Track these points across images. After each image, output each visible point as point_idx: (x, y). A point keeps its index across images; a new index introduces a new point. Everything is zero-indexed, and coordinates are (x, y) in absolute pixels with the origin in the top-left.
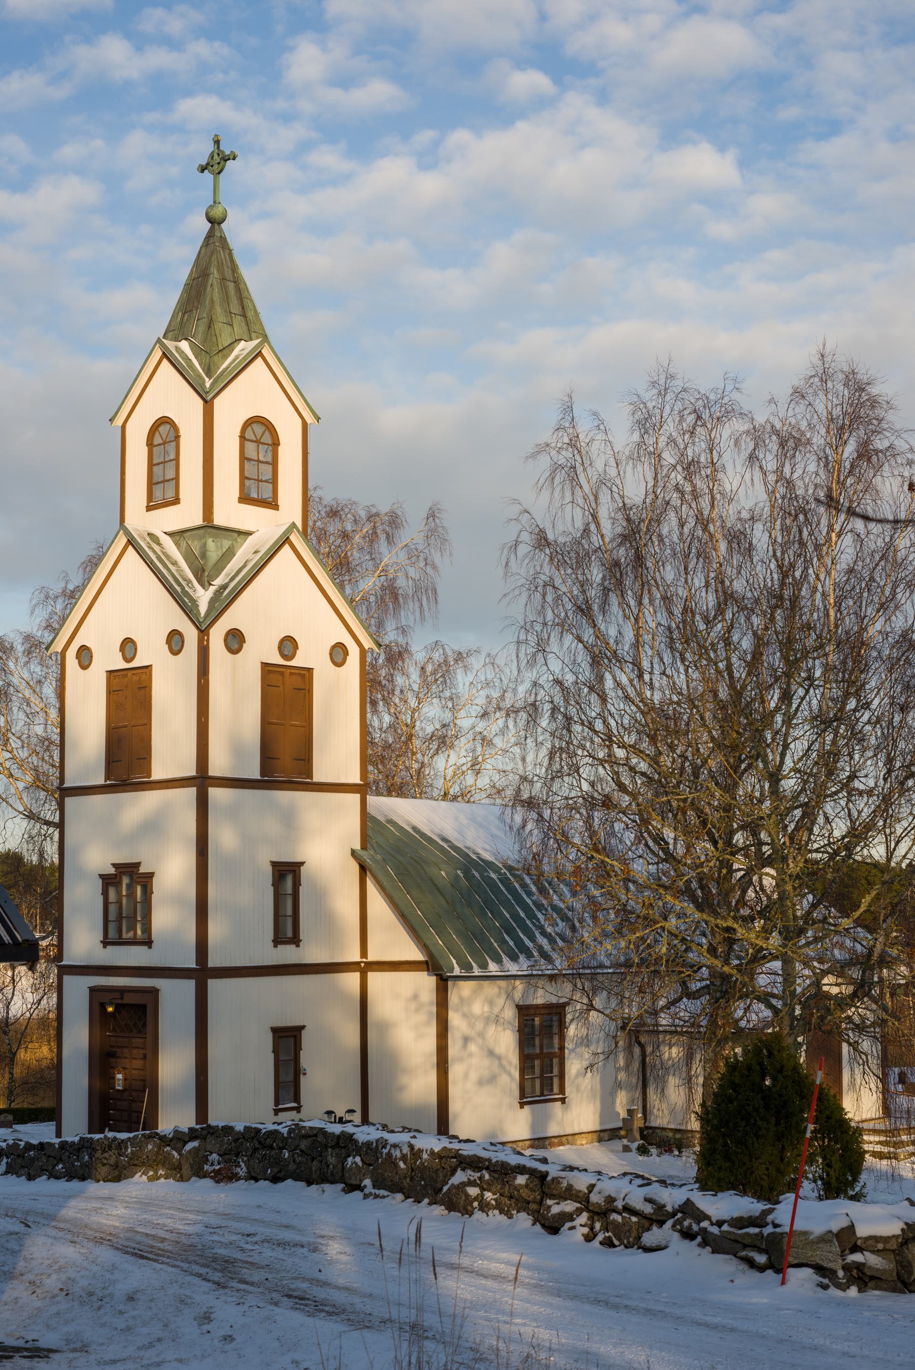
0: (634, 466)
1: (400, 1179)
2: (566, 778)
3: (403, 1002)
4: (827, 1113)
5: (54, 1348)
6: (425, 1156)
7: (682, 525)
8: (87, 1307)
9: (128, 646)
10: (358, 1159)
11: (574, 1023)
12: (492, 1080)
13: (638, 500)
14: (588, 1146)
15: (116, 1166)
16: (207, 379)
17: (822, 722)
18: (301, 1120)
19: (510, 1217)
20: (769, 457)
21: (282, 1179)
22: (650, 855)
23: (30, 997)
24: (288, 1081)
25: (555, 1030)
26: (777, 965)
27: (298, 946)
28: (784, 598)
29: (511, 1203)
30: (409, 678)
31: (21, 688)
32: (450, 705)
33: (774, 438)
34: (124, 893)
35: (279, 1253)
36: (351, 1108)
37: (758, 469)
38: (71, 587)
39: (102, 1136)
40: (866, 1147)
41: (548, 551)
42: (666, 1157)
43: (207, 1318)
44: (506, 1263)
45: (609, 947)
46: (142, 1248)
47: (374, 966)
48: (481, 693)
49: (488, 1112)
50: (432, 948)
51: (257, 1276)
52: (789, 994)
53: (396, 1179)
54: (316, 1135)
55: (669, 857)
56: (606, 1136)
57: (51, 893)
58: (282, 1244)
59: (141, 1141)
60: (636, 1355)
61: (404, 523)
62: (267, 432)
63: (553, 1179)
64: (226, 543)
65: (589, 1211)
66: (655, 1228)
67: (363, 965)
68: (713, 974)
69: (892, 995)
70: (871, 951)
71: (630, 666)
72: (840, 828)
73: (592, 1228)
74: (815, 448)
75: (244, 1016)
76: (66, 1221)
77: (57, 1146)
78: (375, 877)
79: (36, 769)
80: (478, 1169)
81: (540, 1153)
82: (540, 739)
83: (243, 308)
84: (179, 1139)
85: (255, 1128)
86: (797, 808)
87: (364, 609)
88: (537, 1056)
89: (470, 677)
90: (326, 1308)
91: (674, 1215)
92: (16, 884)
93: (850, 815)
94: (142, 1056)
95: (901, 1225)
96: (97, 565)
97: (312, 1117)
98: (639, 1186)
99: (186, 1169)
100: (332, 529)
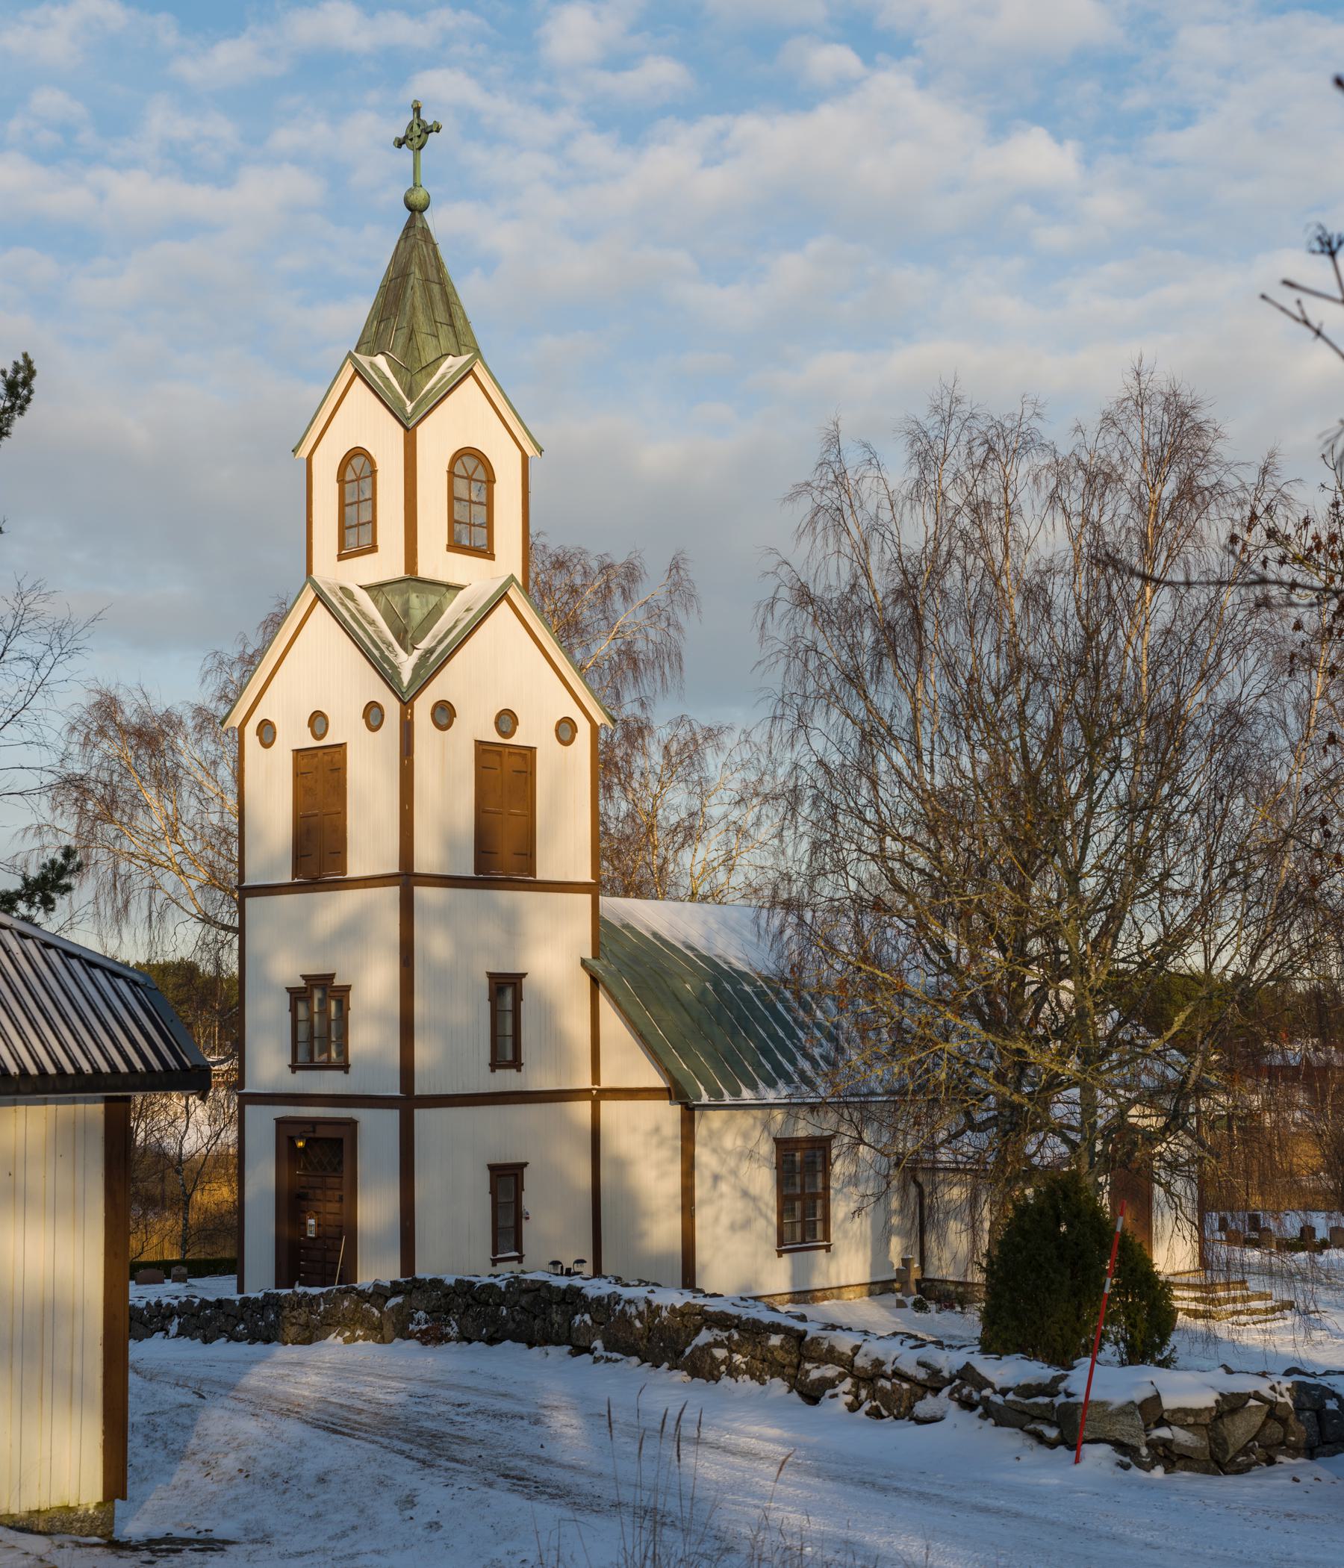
0: (912, 508)
2: (830, 876)
3: (641, 1133)
4: (1132, 1264)
5: (231, 1539)
6: (664, 1314)
7: (966, 578)
8: (270, 1491)
9: (318, 721)
10: (587, 1317)
12: (746, 1224)
13: (917, 548)
15: (306, 1326)
16: (408, 402)
17: (1131, 809)
18: (523, 1272)
19: (763, 1383)
20: (1074, 496)
21: (500, 1341)
23: (206, 1130)
25: (819, 1167)
26: (1075, 1093)
27: (519, 1070)
28: (1088, 663)
29: (764, 1367)
31: (192, 769)
32: (698, 790)
33: (1080, 473)
35: (494, 1426)
37: (1060, 511)
38: (250, 651)
39: (290, 1291)
40: (1177, 1304)
42: (947, 1313)
43: (409, 1502)
44: (757, 1438)
45: (880, 1073)
46: (335, 1421)
48: (736, 775)
49: (740, 1259)
50: (674, 1072)
51: (469, 1453)
52: (1088, 1125)
54: (538, 1290)
55: (951, 967)
57: (230, 1009)
58: (498, 1416)
60: (911, 1547)
63: (813, 1339)
64: (433, 600)
65: (853, 1376)
66: (929, 1396)
68: (1003, 1103)
69: (1212, 1128)
70: (1186, 1076)
71: (908, 745)
72: (1151, 934)
73: (857, 1396)
74: (1129, 486)
76: (247, 1390)
79: (211, 865)
80: (727, 1328)
81: (798, 1309)
82: (801, 829)
84: (380, 1294)
86: (1100, 910)
87: (597, 678)
88: (797, 1197)
90: (549, 1490)
91: (951, 1381)
92: (189, 999)
93: (1163, 919)
95: (1216, 1396)
96: (279, 625)
97: (535, 1269)
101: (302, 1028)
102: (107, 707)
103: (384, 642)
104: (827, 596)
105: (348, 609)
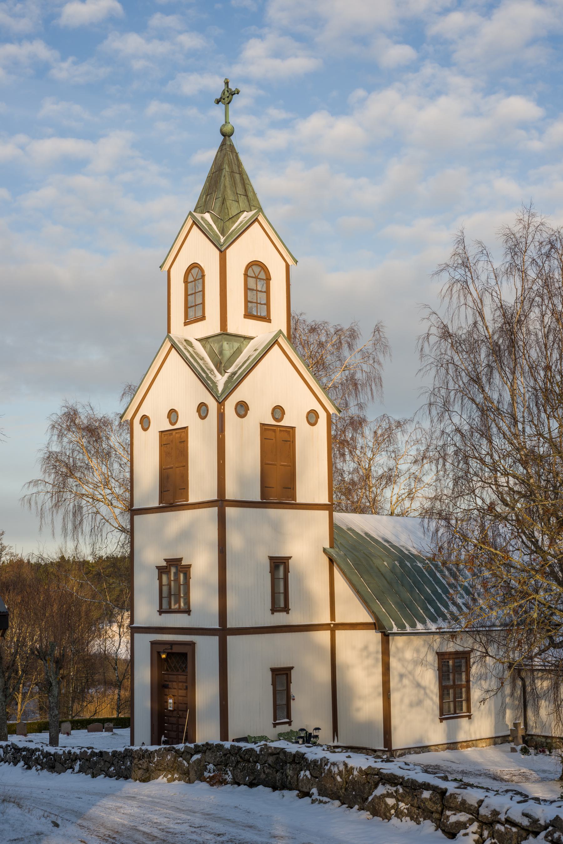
1: (337, 789)
3: (357, 652)
6: (355, 773)
9: (173, 414)
10: (308, 773)
11: (476, 664)
12: (419, 703)
14: (488, 747)
15: (147, 770)
16: (222, 237)
19: (419, 823)
22: (526, 549)
24: (282, 705)
25: (464, 669)
27: (288, 613)
29: (420, 812)
30: (366, 438)
32: (393, 455)
34: (172, 579)
36: (317, 727)
41: (450, 341)
42: (541, 756)
47: (340, 627)
48: (414, 447)
50: (377, 613)
53: (335, 789)
54: (278, 754)
55: (538, 549)
56: (499, 741)
59: (163, 753)
61: (359, 336)
62: (262, 271)
63: (451, 795)
64: (236, 345)
65: (479, 821)
66: (531, 837)
67: (332, 625)
73: (481, 835)
75: (252, 659)
76: (90, 819)
77: (110, 754)
78: (339, 566)
80: (396, 785)
83: (245, 190)
85: (238, 747)
89: (406, 438)
91: (546, 828)
94: (185, 688)
98: (518, 802)
99: (192, 775)
100: (311, 340)
101: (165, 589)
102: (71, 416)
103: (208, 369)
104: (460, 333)
105: (189, 352)
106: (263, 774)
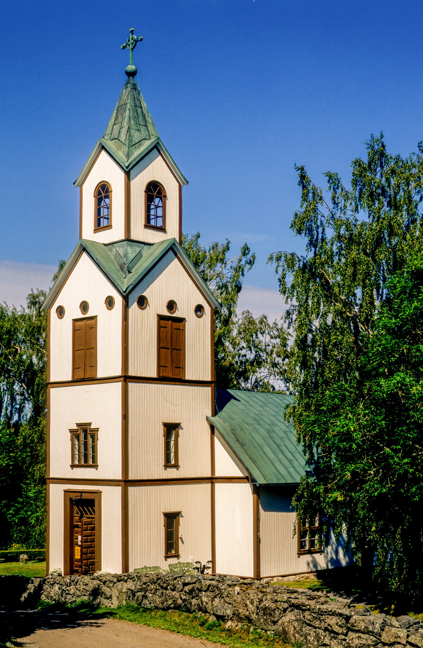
64: (138, 250)
106: (179, 599)
